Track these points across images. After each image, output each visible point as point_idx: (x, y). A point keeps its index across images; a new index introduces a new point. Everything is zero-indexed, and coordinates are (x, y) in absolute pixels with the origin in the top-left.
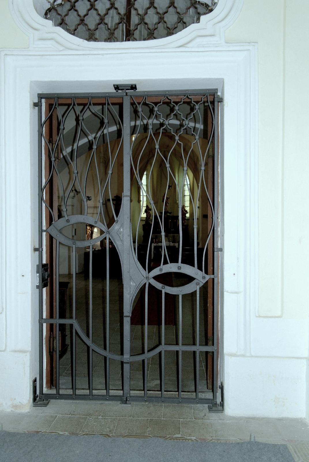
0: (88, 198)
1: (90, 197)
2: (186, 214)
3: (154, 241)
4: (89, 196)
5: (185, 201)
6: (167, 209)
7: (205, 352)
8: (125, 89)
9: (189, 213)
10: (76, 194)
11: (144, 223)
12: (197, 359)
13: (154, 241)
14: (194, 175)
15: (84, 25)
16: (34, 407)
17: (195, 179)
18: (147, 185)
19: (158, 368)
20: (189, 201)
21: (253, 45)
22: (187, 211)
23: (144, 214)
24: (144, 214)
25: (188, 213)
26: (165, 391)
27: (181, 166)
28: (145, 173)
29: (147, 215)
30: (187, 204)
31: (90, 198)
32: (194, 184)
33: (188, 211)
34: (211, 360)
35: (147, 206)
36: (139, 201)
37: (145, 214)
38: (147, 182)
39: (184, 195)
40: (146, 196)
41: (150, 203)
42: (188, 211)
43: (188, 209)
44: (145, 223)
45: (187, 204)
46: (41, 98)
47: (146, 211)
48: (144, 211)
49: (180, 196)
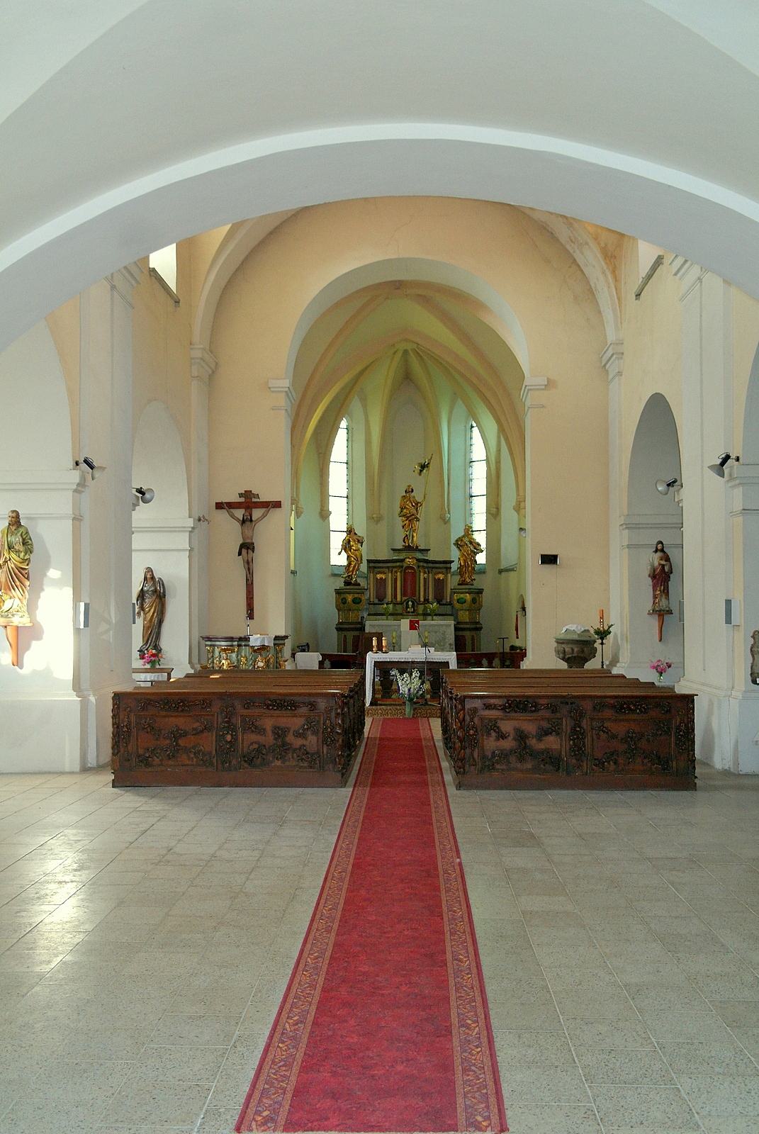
2: (476, 554)
4: (144, 488)
5: (471, 515)
6: (415, 539)
9: (484, 552)
14: (502, 430)
17: (502, 439)
19: (306, 921)
22: (479, 545)
23: (340, 554)
24: (340, 554)
25: (482, 551)
26: (345, 636)
27: (460, 402)
28: (344, 424)
30: (479, 521)
31: (147, 496)
32: (503, 466)
35: (350, 531)
36: (324, 514)
37: (344, 555)
39: (468, 461)
40: (347, 497)
41: (348, 431)
42: (483, 546)
43: (480, 538)
47: (346, 546)
49: (456, 497)
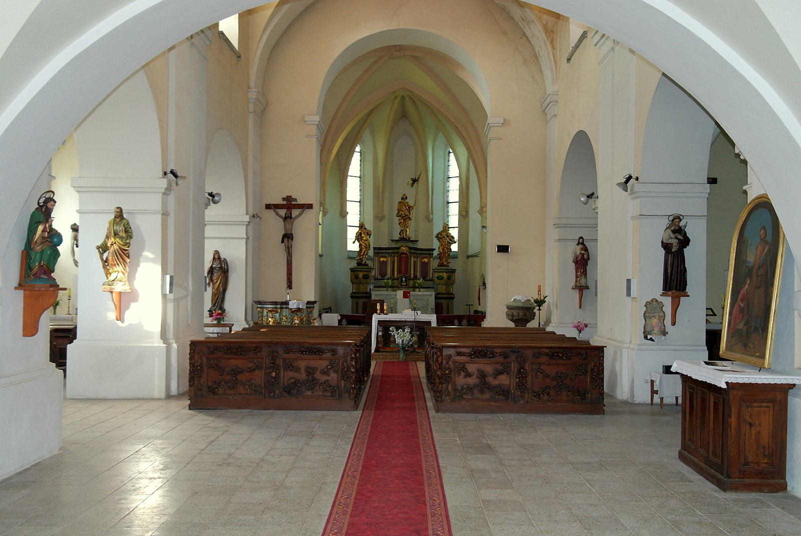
0: (211, 198)
1: (219, 194)
2: (451, 244)
3: (378, 307)
4: (214, 193)
5: (448, 216)
9: (457, 243)
10: (174, 184)
11: (354, 264)
12: (734, 494)
13: (378, 307)
15: (431, 390)
18: (362, 177)
21: (607, 39)
23: (354, 243)
24: (354, 243)
25: (455, 242)
28: (358, 149)
29: (360, 245)
30: (454, 221)
31: (216, 198)
34: (248, 314)
35: (361, 226)
37: (357, 243)
39: (446, 177)
43: (454, 233)
46: (285, 237)
47: (359, 237)
49: (437, 202)
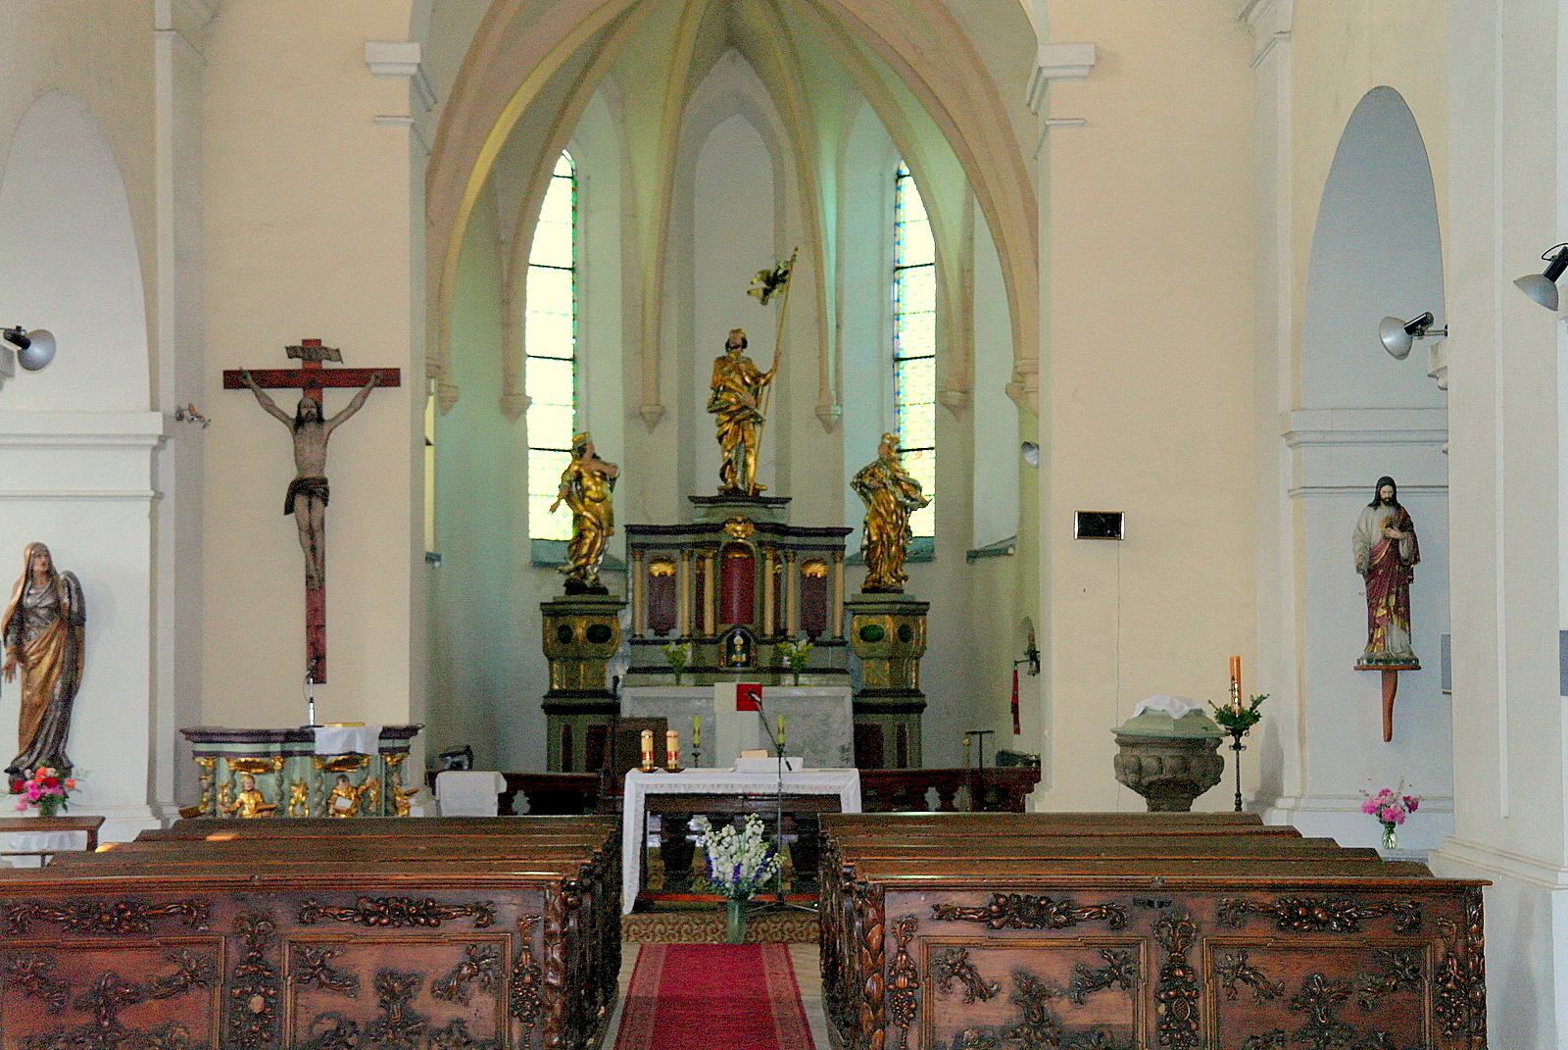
1: (44, 335)
7: (719, 761)
8: (674, 643)
9: (931, 507)
11: (553, 587)
16: (788, 496)
20: (932, 407)
23: (553, 509)
24: (553, 509)
25: (924, 504)
28: (564, 165)
30: (918, 425)
31: (36, 350)
33: (928, 490)
37: (566, 512)
38: (581, 242)
43: (920, 469)
44: (934, 789)
45: (918, 425)
47: (572, 490)
48: (557, 492)
